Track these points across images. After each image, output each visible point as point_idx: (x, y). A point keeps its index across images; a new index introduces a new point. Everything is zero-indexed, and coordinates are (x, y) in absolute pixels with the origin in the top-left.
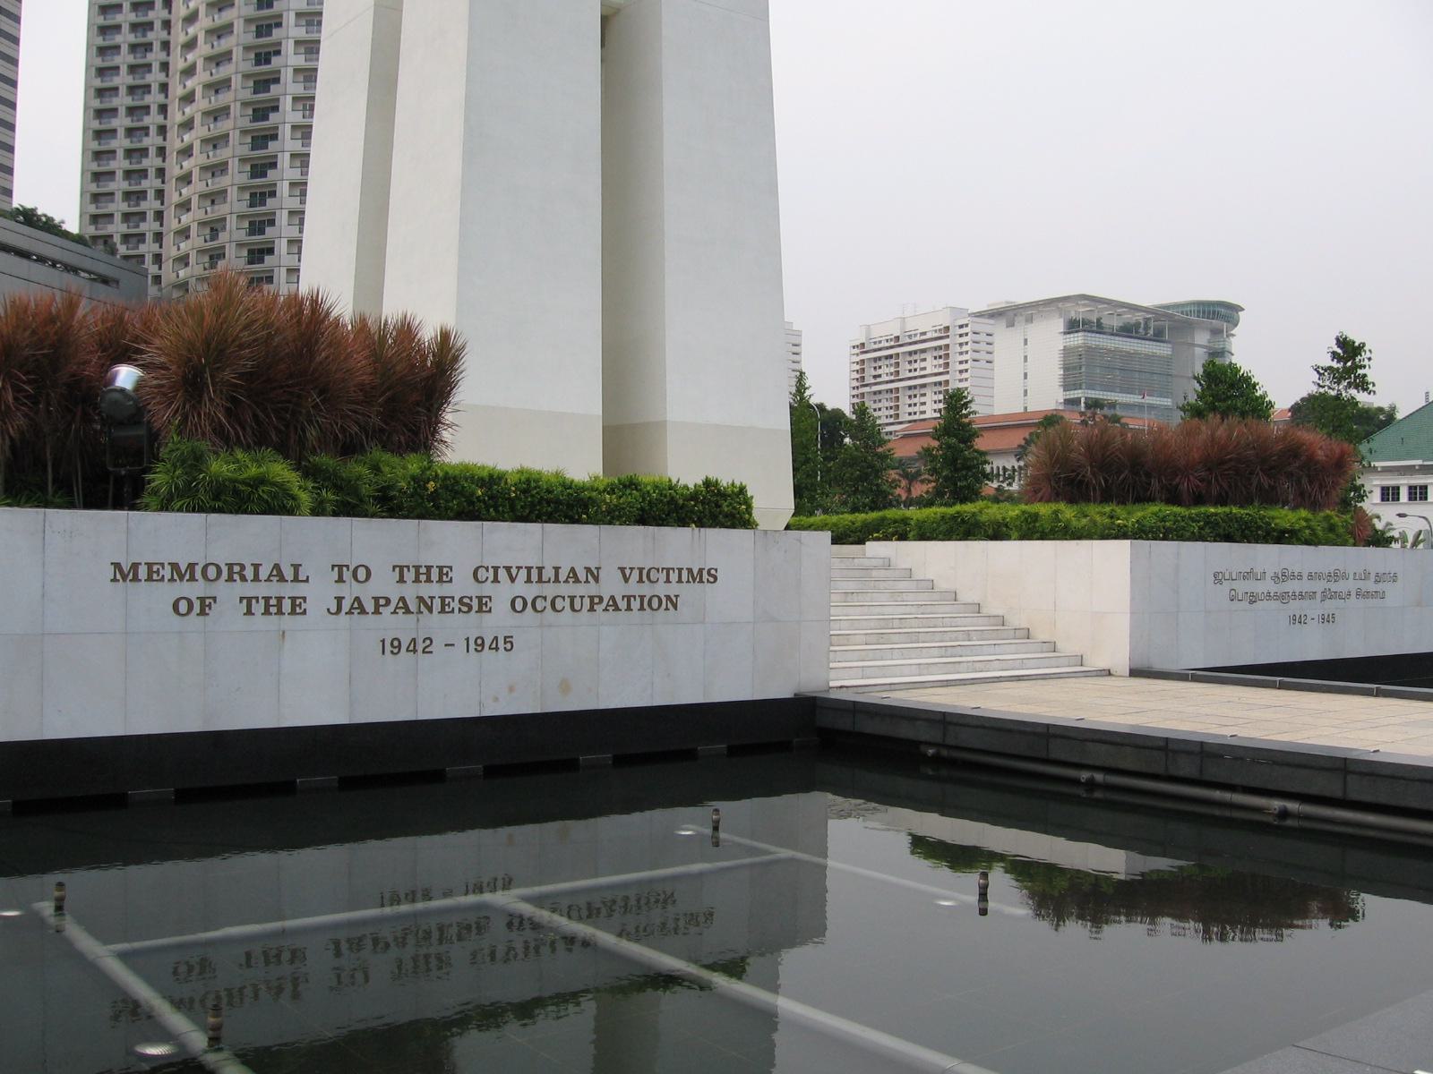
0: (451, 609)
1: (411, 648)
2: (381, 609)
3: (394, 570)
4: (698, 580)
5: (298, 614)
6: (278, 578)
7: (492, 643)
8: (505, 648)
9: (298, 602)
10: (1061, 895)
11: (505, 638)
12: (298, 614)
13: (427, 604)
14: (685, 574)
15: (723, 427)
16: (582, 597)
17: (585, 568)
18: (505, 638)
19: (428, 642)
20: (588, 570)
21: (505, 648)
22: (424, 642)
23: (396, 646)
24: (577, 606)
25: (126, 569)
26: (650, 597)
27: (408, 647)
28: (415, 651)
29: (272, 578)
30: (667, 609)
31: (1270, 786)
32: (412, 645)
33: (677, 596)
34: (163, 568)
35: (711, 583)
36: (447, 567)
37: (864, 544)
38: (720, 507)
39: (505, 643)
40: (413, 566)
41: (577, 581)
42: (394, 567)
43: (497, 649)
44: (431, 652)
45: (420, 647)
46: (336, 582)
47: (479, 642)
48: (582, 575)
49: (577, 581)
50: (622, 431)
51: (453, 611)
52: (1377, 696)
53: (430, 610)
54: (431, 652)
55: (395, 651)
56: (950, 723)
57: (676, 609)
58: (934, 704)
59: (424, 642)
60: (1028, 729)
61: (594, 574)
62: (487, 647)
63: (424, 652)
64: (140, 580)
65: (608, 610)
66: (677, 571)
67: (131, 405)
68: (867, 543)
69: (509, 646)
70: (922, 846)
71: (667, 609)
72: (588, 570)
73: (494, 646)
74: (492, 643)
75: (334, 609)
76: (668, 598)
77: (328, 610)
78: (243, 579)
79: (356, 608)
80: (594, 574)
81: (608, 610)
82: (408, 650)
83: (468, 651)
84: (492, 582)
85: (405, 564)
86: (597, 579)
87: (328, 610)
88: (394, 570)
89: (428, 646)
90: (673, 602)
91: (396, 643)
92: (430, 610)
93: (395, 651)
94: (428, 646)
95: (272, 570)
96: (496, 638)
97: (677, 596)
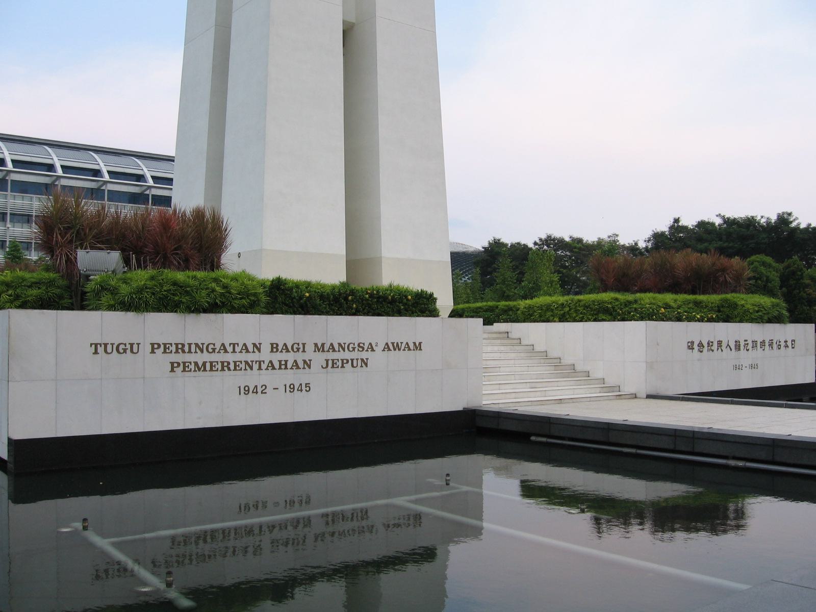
0: (189, 369)
1: (255, 391)
2: (175, 369)
3: (91, 346)
4: (321, 350)
5: (187, 371)
6: (245, 351)
7: (254, 389)
8: (306, 390)
9: (187, 364)
10: (609, 511)
11: (306, 384)
12: (187, 371)
13: (248, 366)
14: (193, 347)
15: (413, 259)
16: (357, 359)
17: (252, 344)
18: (306, 384)
19: (264, 387)
20: (254, 345)
21: (306, 390)
22: (262, 387)
23: (292, 388)
24: (355, 364)
25: (319, 346)
26: (340, 357)
27: (253, 390)
28: (257, 392)
29: (242, 351)
30: (362, 366)
31: (705, 452)
32: (255, 389)
33: (367, 359)
34: (172, 346)
35: (360, 351)
36: (168, 344)
37: (493, 325)
38: (420, 305)
39: (306, 387)
40: (175, 344)
41: (334, 351)
42: (91, 345)
43: (301, 390)
44: (266, 393)
45: (259, 390)
46: (150, 353)
47: (247, 389)
48: (251, 348)
49: (248, 351)
50: (354, 263)
51: (241, 369)
52: (682, 400)
53: (251, 368)
54: (266, 393)
55: (247, 392)
56: (551, 423)
57: (367, 366)
58: (523, 411)
59: (262, 387)
60: (578, 424)
61: (257, 347)
62: (251, 391)
63: (262, 393)
64: (192, 353)
65: (293, 369)
66: (103, 346)
67: (135, 256)
68: (494, 324)
69: (308, 389)
70: (530, 490)
71: (362, 366)
72: (254, 345)
73: (255, 391)
74: (254, 389)
75: (324, 366)
76: (362, 360)
77: (322, 366)
78: (184, 352)
79: (294, 366)
80: (257, 347)
81: (293, 369)
82: (298, 390)
83: (240, 394)
84: (302, 352)
85: (237, 343)
86: (259, 350)
87: (322, 366)
88: (91, 346)
89: (264, 390)
90: (365, 363)
91: (292, 386)
92: (251, 368)
93: (292, 390)
94: (264, 390)
95: (283, 347)
96: (301, 384)
97: (367, 359)
